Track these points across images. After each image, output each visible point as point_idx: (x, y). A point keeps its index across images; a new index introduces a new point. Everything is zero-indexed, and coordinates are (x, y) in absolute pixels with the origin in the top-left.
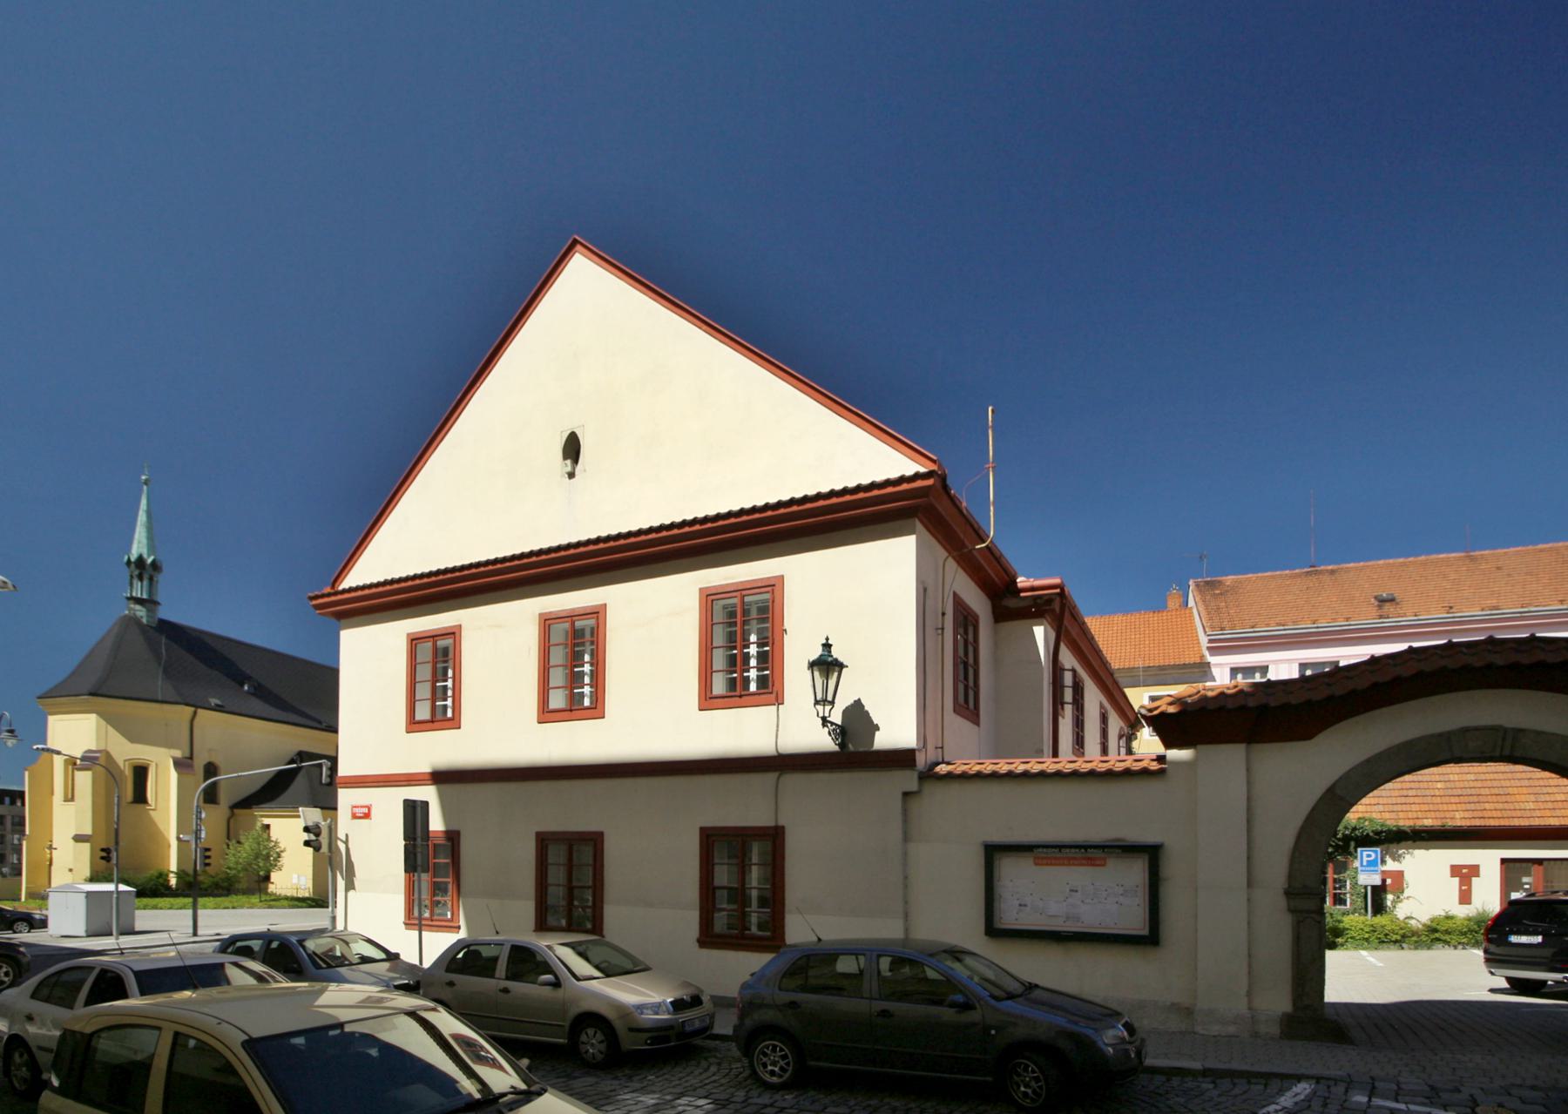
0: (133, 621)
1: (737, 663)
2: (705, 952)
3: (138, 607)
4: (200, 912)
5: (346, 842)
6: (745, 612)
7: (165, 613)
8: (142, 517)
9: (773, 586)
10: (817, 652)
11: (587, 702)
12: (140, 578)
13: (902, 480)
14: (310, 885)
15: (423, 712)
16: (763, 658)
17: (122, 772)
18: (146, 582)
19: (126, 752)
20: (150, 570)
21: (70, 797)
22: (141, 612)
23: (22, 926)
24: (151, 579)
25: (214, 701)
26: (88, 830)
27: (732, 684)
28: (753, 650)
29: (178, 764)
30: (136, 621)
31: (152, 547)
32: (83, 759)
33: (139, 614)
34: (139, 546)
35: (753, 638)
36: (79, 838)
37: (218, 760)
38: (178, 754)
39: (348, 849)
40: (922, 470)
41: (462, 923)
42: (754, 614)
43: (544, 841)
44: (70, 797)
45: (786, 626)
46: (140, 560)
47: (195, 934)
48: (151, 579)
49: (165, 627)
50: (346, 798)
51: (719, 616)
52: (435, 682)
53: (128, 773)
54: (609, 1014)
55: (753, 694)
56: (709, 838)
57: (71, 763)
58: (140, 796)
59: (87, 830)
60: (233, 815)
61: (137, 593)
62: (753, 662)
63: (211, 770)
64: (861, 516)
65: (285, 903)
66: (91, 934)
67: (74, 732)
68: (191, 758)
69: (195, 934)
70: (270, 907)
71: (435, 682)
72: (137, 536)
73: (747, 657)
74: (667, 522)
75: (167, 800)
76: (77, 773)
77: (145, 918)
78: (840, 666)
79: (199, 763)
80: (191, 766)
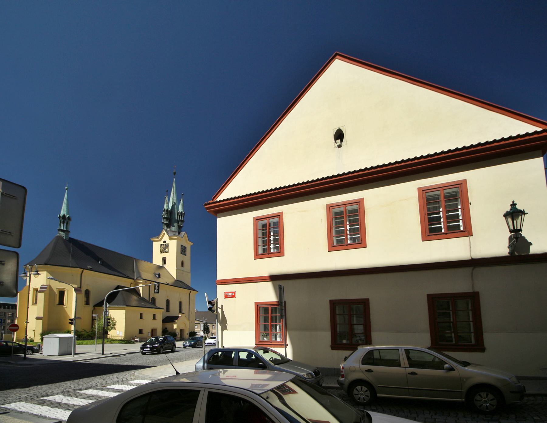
0: (60, 238)
1: (266, 243)
2: (335, 352)
3: (62, 233)
4: (105, 345)
5: (222, 309)
6: (270, 225)
7: (71, 235)
8: (65, 201)
9: (279, 216)
10: (508, 208)
11: (462, 229)
12: (64, 223)
13: (527, 134)
14: (124, 335)
15: (260, 251)
16: (276, 241)
17: (55, 293)
18: (65, 224)
19: (57, 286)
20: (67, 220)
21: (35, 302)
22: (63, 235)
23: (30, 352)
24: (67, 223)
25: (89, 267)
26: (42, 315)
27: (264, 250)
28: (272, 238)
29: (76, 290)
30: (61, 238)
31: (68, 213)
32: (41, 288)
33: (63, 235)
34: (64, 211)
35: (272, 234)
36: (38, 318)
37: (90, 288)
38: (76, 286)
39: (223, 312)
40: (539, 129)
41: (288, 342)
42: (272, 226)
43: (334, 304)
44: (35, 302)
45: (470, 200)
46: (64, 216)
47: (103, 354)
48: (67, 223)
49: (71, 240)
50: (221, 290)
51: (260, 227)
52: (269, 240)
53: (57, 293)
54: (492, 382)
55: (443, 234)
56: (334, 304)
57: (36, 290)
58: (61, 302)
59: (41, 315)
60: (94, 309)
61: (62, 228)
62: (272, 242)
63: (87, 293)
64: (370, 178)
65: (117, 342)
66: (60, 355)
67: (39, 280)
68: (81, 288)
69: (103, 354)
70: (112, 343)
71: (269, 240)
72: (63, 208)
73: (270, 241)
74: (237, 196)
75: (72, 303)
76: (39, 294)
77: (79, 348)
78: (523, 213)
79: (83, 289)
80: (81, 291)
